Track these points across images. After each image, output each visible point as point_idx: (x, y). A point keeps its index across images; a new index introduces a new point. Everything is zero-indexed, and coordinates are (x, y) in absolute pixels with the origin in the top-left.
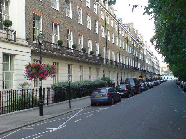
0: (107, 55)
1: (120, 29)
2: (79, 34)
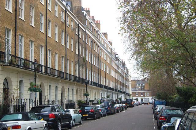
0: (15, 47)
1: (80, 34)
2: (6, 28)
